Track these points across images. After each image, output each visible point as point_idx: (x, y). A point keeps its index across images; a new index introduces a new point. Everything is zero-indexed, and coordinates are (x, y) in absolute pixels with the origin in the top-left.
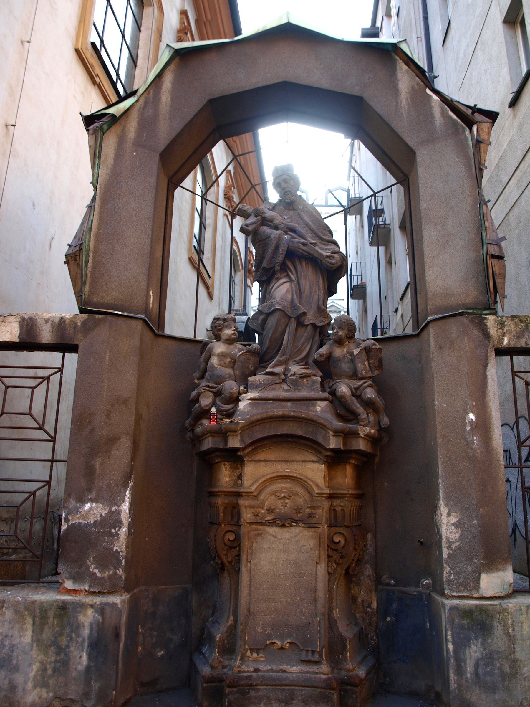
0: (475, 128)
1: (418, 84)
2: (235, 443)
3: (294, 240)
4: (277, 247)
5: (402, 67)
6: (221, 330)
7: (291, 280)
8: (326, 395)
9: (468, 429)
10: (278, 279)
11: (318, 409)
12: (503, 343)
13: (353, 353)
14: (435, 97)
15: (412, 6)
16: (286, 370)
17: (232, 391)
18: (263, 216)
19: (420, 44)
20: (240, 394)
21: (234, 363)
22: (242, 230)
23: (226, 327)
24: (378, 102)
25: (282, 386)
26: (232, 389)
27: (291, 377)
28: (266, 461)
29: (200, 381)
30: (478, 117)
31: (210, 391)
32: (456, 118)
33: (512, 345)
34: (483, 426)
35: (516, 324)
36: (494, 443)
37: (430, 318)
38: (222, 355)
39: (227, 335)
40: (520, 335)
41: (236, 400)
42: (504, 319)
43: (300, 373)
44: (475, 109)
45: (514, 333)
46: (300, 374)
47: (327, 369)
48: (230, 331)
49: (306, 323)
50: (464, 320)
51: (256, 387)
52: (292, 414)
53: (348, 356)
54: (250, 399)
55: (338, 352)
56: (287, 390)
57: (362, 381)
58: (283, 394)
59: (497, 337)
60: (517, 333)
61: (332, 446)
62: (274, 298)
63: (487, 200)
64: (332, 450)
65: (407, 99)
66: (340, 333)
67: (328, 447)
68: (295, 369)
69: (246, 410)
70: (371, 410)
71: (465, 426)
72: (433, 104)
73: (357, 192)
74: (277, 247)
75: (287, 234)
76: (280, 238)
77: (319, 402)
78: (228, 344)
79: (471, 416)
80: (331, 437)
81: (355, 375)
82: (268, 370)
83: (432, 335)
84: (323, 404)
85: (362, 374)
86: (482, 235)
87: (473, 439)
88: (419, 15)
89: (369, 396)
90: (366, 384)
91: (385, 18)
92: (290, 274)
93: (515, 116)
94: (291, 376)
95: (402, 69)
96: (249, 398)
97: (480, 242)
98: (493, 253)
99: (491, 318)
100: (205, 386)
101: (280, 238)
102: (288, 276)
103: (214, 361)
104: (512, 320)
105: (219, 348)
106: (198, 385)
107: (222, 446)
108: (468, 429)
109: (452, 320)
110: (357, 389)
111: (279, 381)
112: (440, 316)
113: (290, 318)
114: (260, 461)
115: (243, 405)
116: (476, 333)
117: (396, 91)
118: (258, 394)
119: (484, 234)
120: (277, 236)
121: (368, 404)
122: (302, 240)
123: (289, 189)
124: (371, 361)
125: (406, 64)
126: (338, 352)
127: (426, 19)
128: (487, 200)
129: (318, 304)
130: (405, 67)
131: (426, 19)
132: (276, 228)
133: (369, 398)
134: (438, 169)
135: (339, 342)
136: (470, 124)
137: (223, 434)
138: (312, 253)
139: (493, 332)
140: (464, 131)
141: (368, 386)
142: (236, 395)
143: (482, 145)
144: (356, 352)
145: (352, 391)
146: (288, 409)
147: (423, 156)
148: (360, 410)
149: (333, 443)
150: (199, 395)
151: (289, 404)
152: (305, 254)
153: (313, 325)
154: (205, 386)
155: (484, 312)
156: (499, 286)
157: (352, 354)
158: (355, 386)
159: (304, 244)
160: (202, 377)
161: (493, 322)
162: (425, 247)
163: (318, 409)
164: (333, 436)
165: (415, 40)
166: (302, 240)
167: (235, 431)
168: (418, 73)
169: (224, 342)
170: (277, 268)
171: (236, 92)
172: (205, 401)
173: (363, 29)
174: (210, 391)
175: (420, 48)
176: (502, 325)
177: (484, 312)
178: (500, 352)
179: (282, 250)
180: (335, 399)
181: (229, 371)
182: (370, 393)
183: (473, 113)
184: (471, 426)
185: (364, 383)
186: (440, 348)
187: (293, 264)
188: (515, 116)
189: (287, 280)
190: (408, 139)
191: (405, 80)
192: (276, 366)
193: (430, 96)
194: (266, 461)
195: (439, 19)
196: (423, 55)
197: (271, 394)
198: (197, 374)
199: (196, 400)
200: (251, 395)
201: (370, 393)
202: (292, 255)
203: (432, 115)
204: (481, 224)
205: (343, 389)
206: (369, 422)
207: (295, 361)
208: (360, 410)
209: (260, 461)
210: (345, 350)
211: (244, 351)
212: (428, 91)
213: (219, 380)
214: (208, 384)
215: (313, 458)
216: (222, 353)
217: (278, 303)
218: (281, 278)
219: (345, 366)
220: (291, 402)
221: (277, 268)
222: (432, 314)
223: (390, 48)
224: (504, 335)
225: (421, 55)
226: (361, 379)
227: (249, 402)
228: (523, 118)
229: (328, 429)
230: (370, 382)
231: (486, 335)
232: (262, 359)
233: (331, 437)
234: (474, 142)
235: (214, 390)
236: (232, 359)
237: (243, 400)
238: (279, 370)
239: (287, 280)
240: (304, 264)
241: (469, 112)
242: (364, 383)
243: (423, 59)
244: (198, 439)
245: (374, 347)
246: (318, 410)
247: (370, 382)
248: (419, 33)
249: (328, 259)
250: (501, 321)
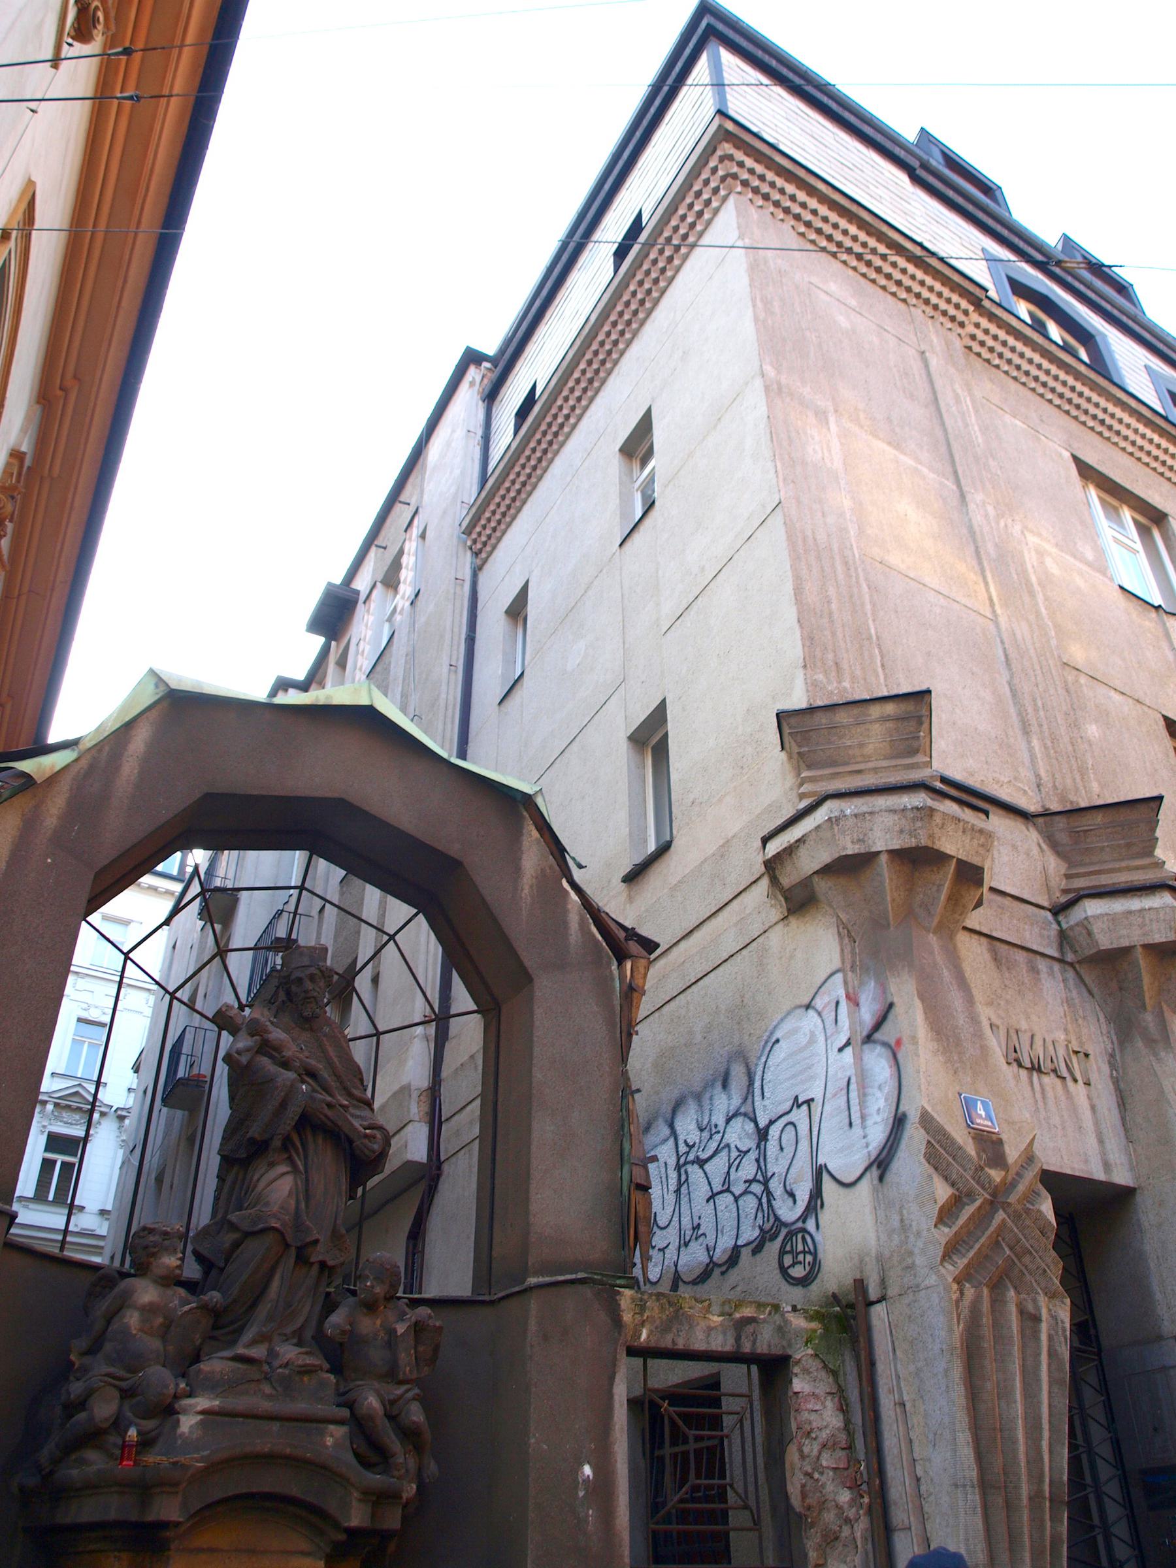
0: (629, 965)
1: (551, 867)
2: (168, 1509)
3: (315, 1094)
4: (284, 1105)
5: (531, 833)
6: (153, 1255)
7: (295, 1169)
8: (345, 1413)
9: (581, 1494)
10: (272, 1165)
11: (329, 1441)
12: (639, 1337)
13: (395, 1331)
14: (574, 896)
15: (450, 606)
16: (272, 1353)
17: (165, 1391)
18: (266, 1036)
19: (453, 676)
20: (176, 1397)
21: (169, 1326)
22: (228, 1059)
23: (166, 1249)
24: (486, 875)
25: (261, 1387)
26: (167, 1387)
27: (280, 1370)
28: (211, 1550)
29: (87, 1360)
30: (634, 947)
31: (115, 1386)
32: (600, 938)
33: (652, 1344)
34: (603, 1487)
35: (662, 1309)
36: (618, 1521)
37: (533, 1280)
38: (149, 1310)
39: (168, 1267)
40: (666, 1328)
41: (169, 1411)
42: (646, 1297)
43: (300, 1362)
44: (632, 934)
45: (658, 1322)
46: (301, 1366)
47: (339, 1356)
48: (173, 1259)
49: (312, 1260)
50: (587, 1291)
51: (213, 1385)
52: (288, 1451)
53: (382, 1334)
54: (202, 1412)
55: (368, 1325)
56: (270, 1397)
57: (403, 1388)
58: (266, 1406)
59: (632, 1326)
60: (662, 1322)
61: (355, 1522)
62: (267, 1204)
63: (634, 1088)
64: (351, 1532)
65: (531, 887)
66: (378, 1290)
67: (346, 1524)
68: (289, 1352)
69: (194, 1436)
70: (411, 1447)
71: (576, 1488)
72: (570, 907)
73: (231, 875)
74: (284, 1105)
75: (303, 1082)
76: (292, 1089)
77: (332, 1427)
78: (163, 1285)
79: (587, 1470)
80: (355, 1503)
81: (391, 1374)
82: (240, 1350)
83: (533, 1312)
84: (339, 1431)
85: (404, 1373)
86: (621, 1145)
87: (587, 1516)
88: (460, 627)
89: (415, 1418)
90: (410, 1395)
91: (379, 585)
92: (294, 1155)
93: (630, 899)
94: (280, 1367)
95: (531, 836)
96: (199, 1408)
97: (618, 1157)
98: (639, 1181)
99: (628, 1293)
100: (105, 1375)
101: (292, 1089)
102: (291, 1160)
103: (133, 1319)
104: (658, 1300)
105: (147, 1293)
106: (85, 1370)
107: (134, 1517)
108: (581, 1494)
109: (569, 1289)
110: (393, 1402)
111: (257, 1376)
112: (547, 1279)
113: (287, 1246)
114: (201, 1550)
115: (187, 1423)
116: (603, 1317)
117: (517, 870)
118: (217, 1403)
119: (627, 1146)
120: (289, 1083)
121: (410, 1435)
122: (329, 1099)
123: (315, 994)
124: (421, 1349)
125: (539, 830)
126: (368, 1325)
127: (471, 640)
128: (634, 1088)
129: (335, 1226)
130: (535, 834)
131: (471, 640)
132: (285, 1064)
133: (414, 1422)
134: (560, 1014)
135: (371, 1307)
136: (622, 957)
137: (145, 1488)
138: (340, 1123)
139: (627, 1317)
140: (609, 964)
141: (414, 1399)
142: (169, 1400)
143: (635, 995)
144: (401, 1329)
145: (384, 1406)
146: (271, 1439)
147: (545, 987)
148: (395, 1444)
149: (357, 1517)
150: (90, 1393)
151: (275, 1426)
152: (329, 1123)
153: (323, 1265)
154: (105, 1375)
155: (618, 1282)
156: (642, 1237)
157: (392, 1332)
158: (392, 1397)
159: (329, 1105)
160: (92, 1351)
161: (629, 1301)
162: (534, 1148)
163: (329, 1441)
164: (360, 1500)
165: (445, 669)
166: (329, 1099)
167: (176, 1485)
168: (554, 848)
169: (155, 1282)
170: (277, 1143)
171: (256, 793)
172: (104, 1409)
173: (329, 584)
174: (115, 1386)
175: (452, 686)
176: (642, 1308)
177: (618, 1282)
178: (632, 1352)
179: (292, 1113)
180: (359, 1424)
181: (155, 1344)
182: (416, 1414)
183: (626, 939)
184: (586, 1489)
185: (407, 1391)
186: (546, 1338)
187: (301, 1139)
188: (630, 899)
189: (289, 1169)
190: (524, 954)
191: (532, 856)
192: (253, 1343)
193: (567, 892)
194: (211, 1550)
195: (500, 657)
196: (455, 698)
197: (241, 1403)
198: (82, 1343)
199: (82, 1404)
200: (202, 1402)
201: (416, 1414)
202: (307, 1122)
203: (565, 924)
204: (623, 1126)
205: (372, 1402)
206: (407, 1471)
207: (285, 1335)
208: (395, 1444)
209: (201, 1550)
210: (378, 1322)
211: (194, 1305)
212: (564, 882)
213: (133, 1362)
214: (112, 1370)
215: (304, 1545)
216: (151, 1304)
217: (274, 1216)
218: (278, 1164)
219: (377, 1355)
220: (278, 1424)
221: (277, 1143)
222: (536, 1274)
223: (519, 797)
224: (643, 1324)
225: (451, 698)
226: (401, 1383)
227: (199, 1417)
228: (647, 911)
229: (353, 1485)
230: (416, 1391)
231: (617, 1321)
232: (222, 1325)
233: (355, 1503)
234: (625, 988)
235: (124, 1384)
236: (165, 1318)
237: (185, 1411)
238: (259, 1352)
239: (289, 1169)
240: (320, 1141)
241: (622, 935)
242: (407, 1391)
243: (454, 705)
244: (60, 1493)
245: (431, 1322)
246: (329, 1444)
247: (416, 1391)
248: (454, 658)
249: (366, 1141)
250: (641, 1300)
